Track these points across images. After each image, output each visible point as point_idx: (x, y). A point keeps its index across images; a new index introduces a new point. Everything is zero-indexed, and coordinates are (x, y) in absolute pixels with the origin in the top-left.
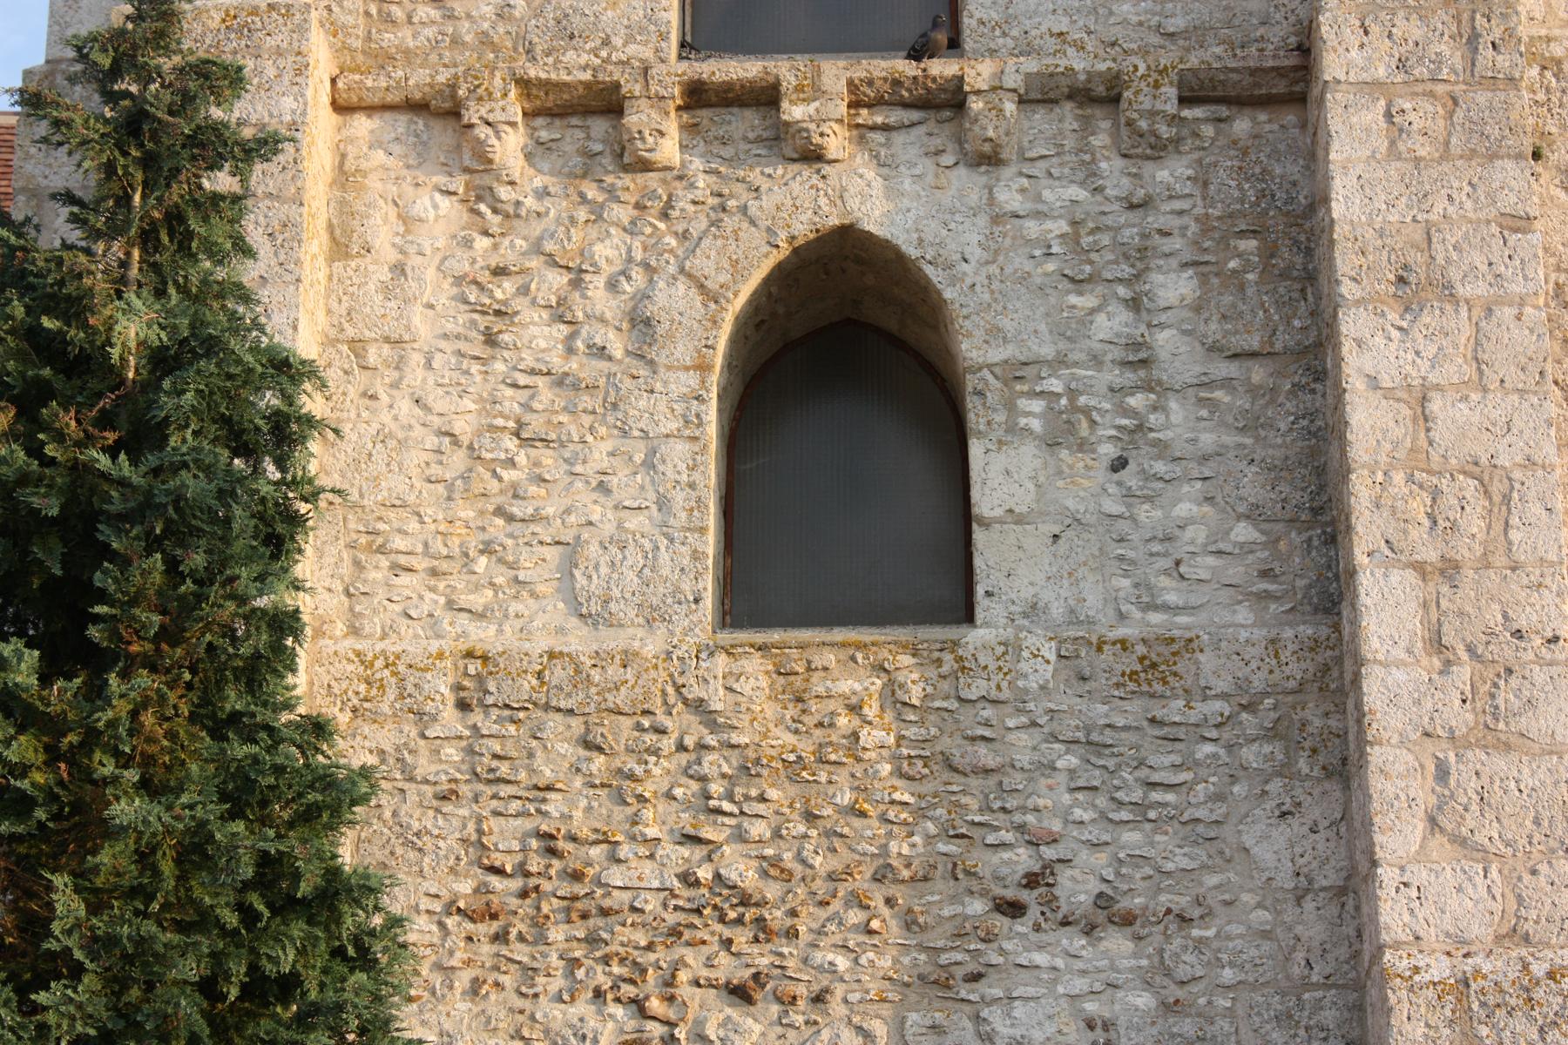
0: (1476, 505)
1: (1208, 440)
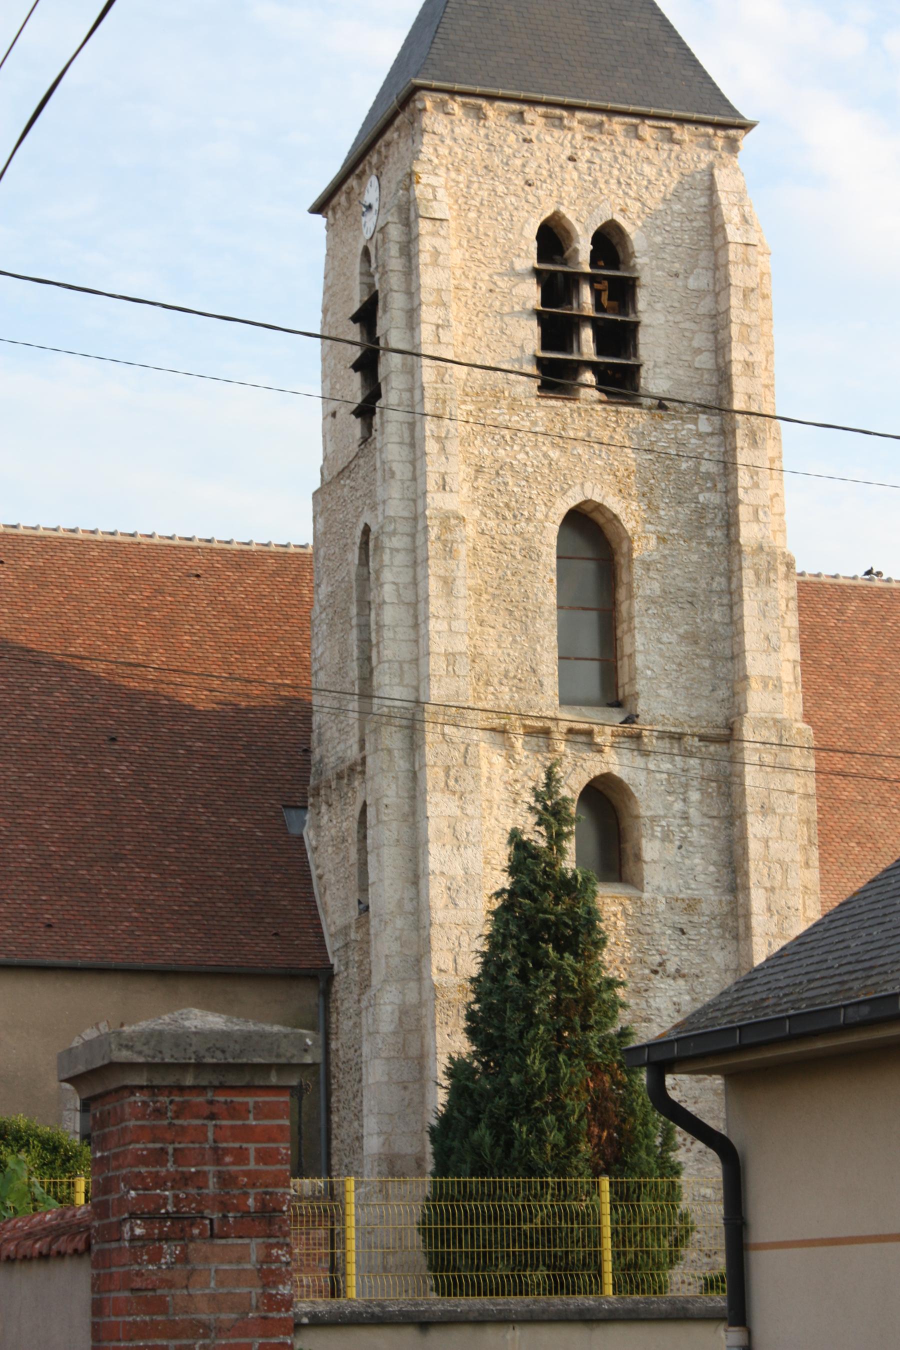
0: (780, 872)
1: (703, 841)
